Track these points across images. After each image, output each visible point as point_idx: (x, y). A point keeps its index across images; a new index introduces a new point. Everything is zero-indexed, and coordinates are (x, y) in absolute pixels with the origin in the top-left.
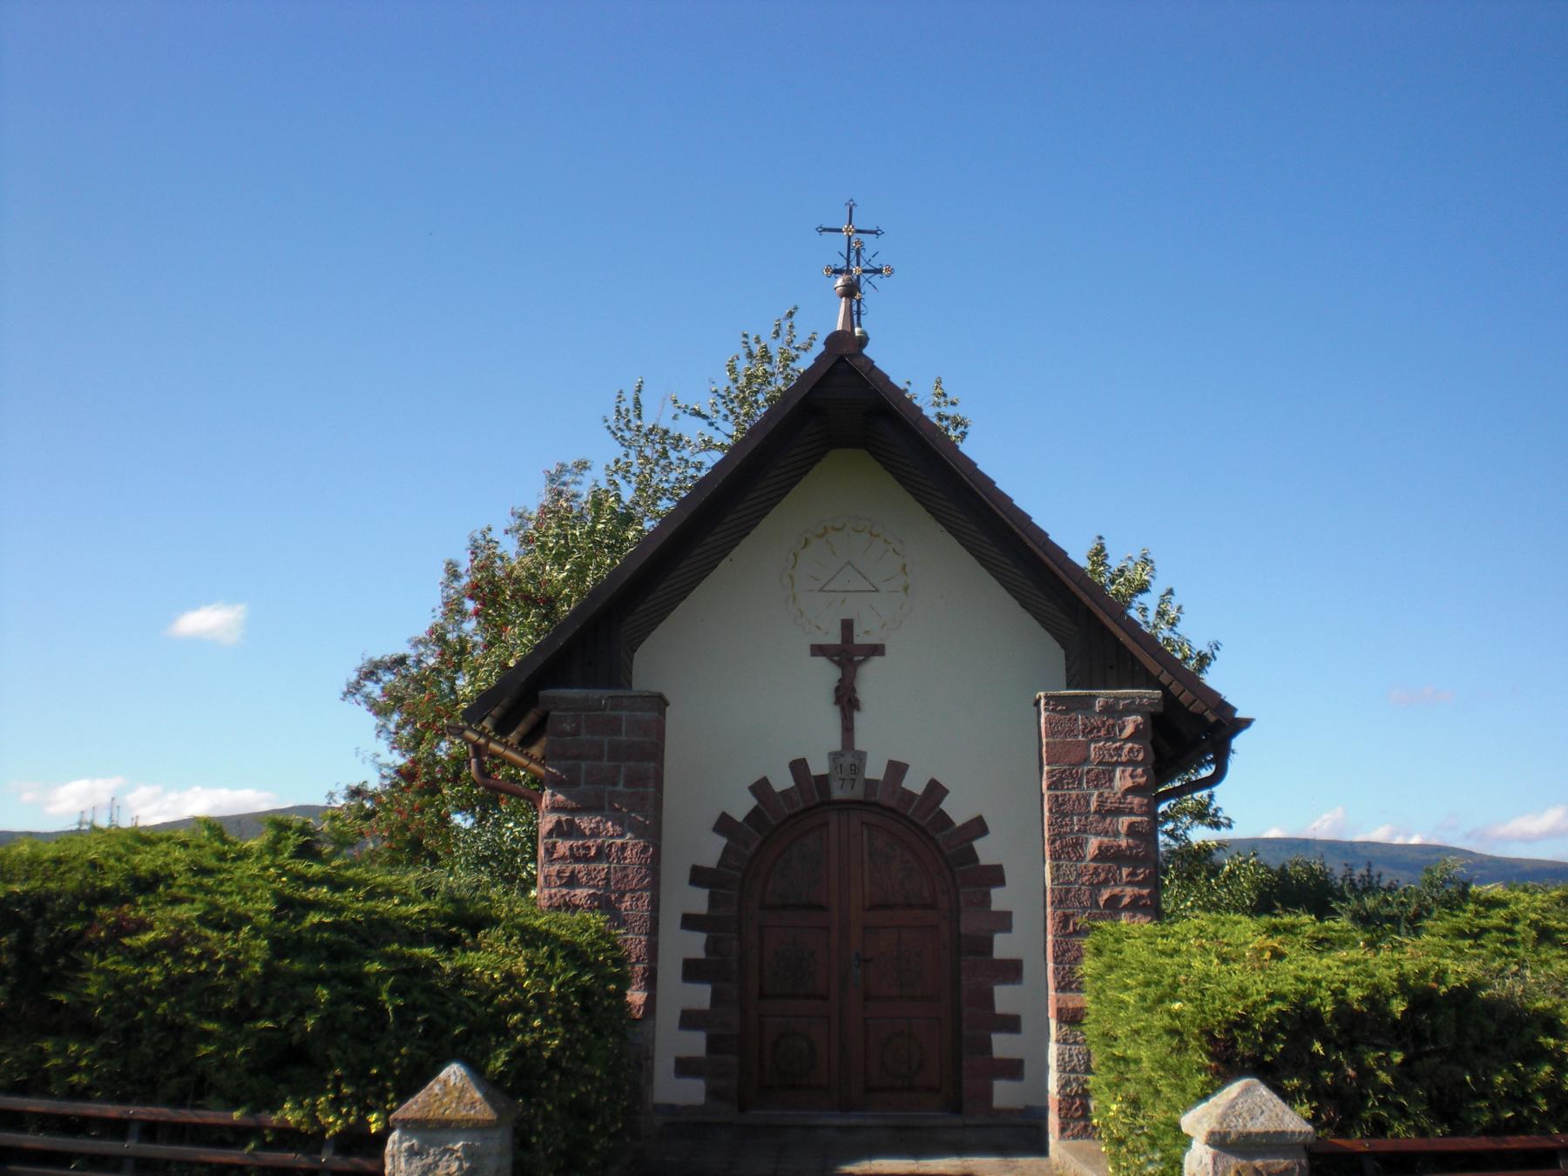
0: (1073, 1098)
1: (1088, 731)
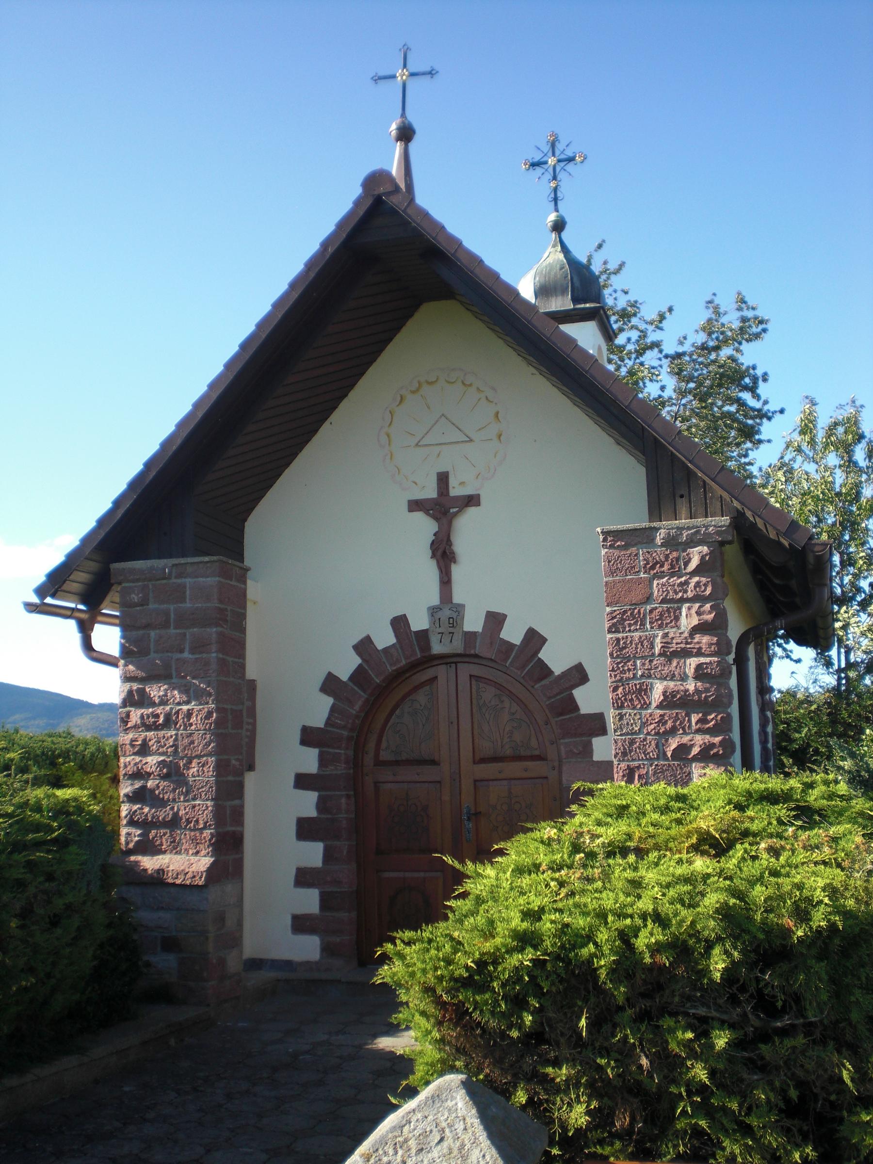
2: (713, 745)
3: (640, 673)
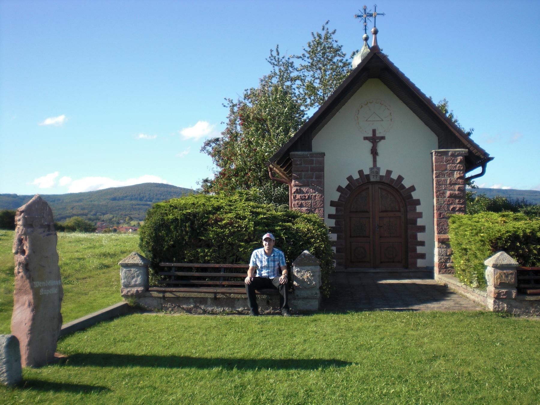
1: (447, 161)
2: (462, 208)
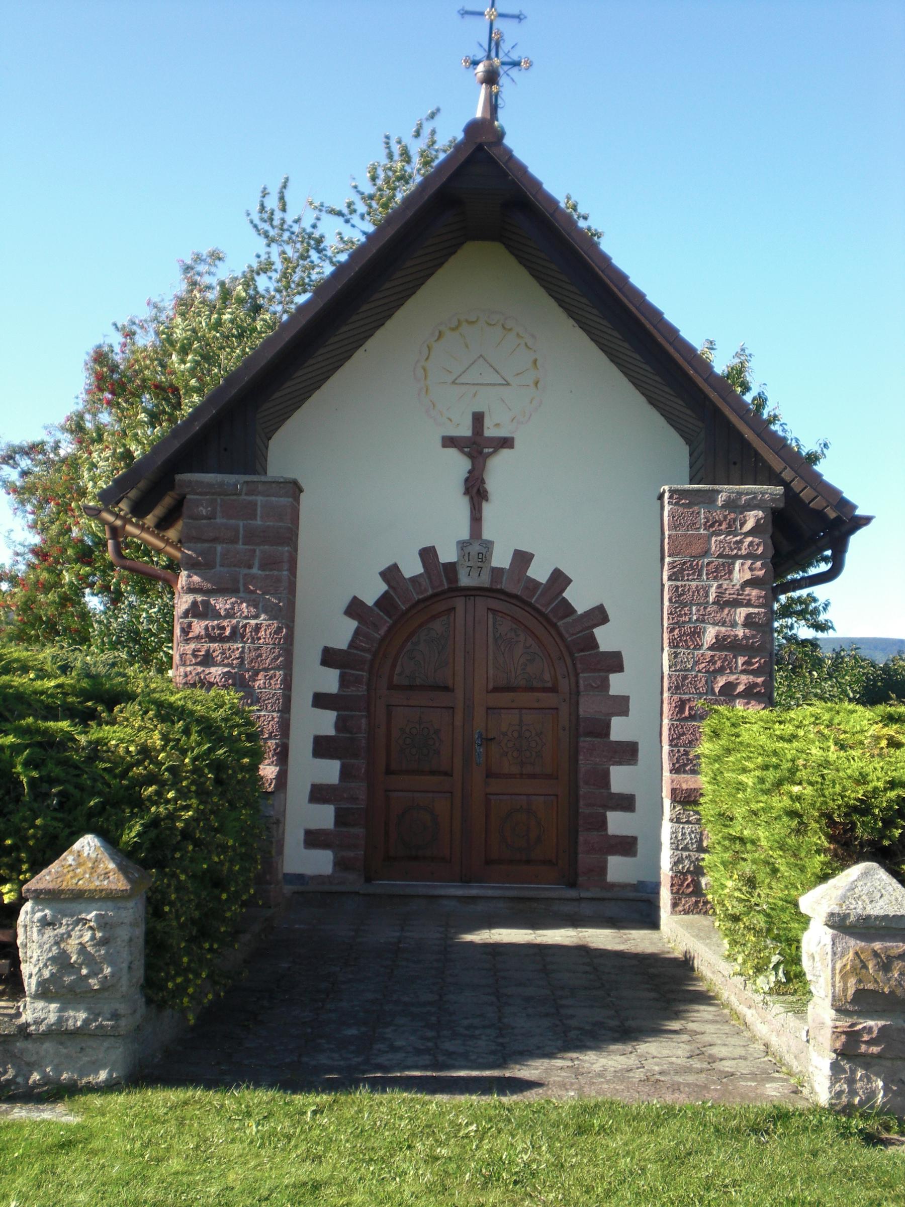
0: (684, 874)
2: (756, 685)
3: (695, 618)
